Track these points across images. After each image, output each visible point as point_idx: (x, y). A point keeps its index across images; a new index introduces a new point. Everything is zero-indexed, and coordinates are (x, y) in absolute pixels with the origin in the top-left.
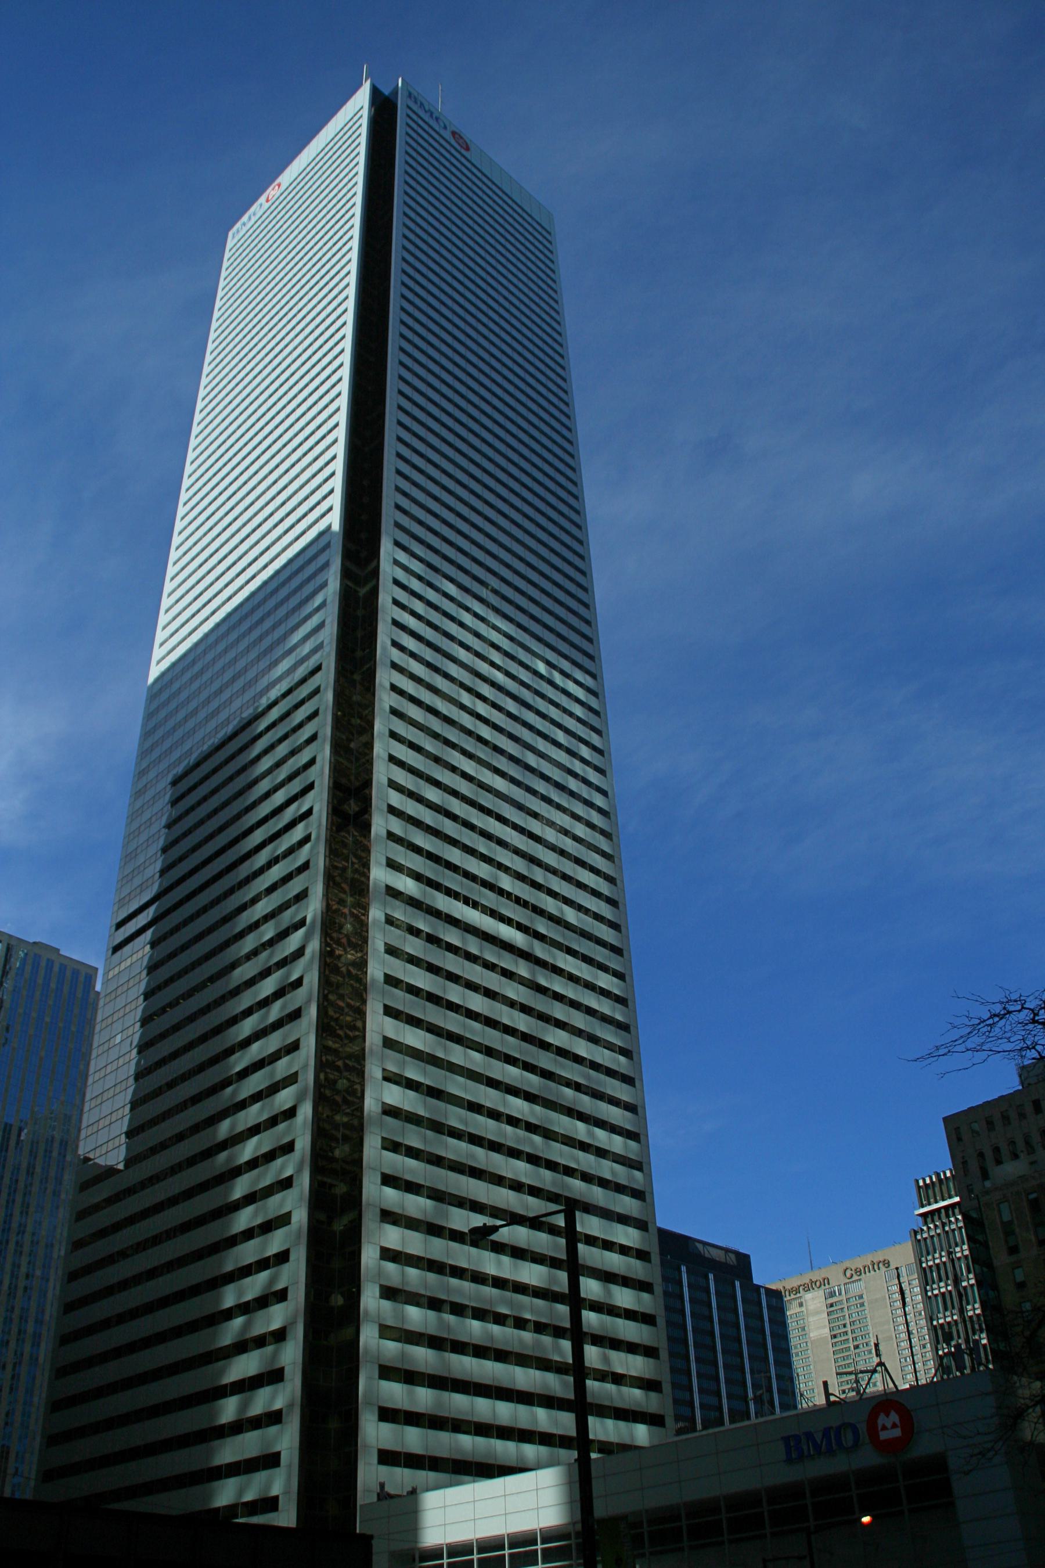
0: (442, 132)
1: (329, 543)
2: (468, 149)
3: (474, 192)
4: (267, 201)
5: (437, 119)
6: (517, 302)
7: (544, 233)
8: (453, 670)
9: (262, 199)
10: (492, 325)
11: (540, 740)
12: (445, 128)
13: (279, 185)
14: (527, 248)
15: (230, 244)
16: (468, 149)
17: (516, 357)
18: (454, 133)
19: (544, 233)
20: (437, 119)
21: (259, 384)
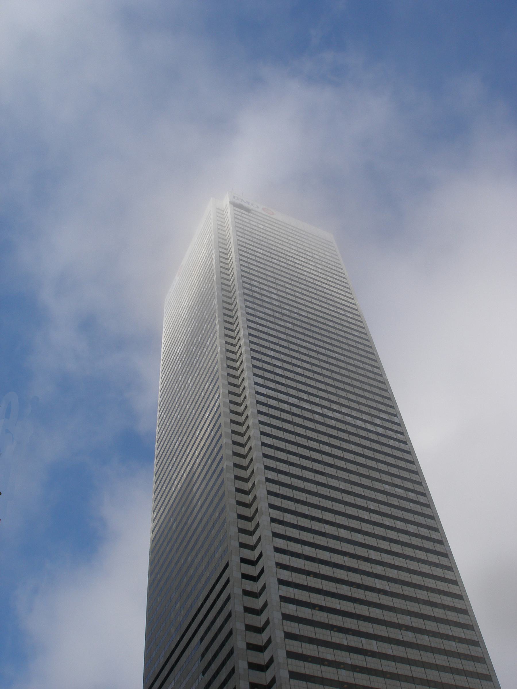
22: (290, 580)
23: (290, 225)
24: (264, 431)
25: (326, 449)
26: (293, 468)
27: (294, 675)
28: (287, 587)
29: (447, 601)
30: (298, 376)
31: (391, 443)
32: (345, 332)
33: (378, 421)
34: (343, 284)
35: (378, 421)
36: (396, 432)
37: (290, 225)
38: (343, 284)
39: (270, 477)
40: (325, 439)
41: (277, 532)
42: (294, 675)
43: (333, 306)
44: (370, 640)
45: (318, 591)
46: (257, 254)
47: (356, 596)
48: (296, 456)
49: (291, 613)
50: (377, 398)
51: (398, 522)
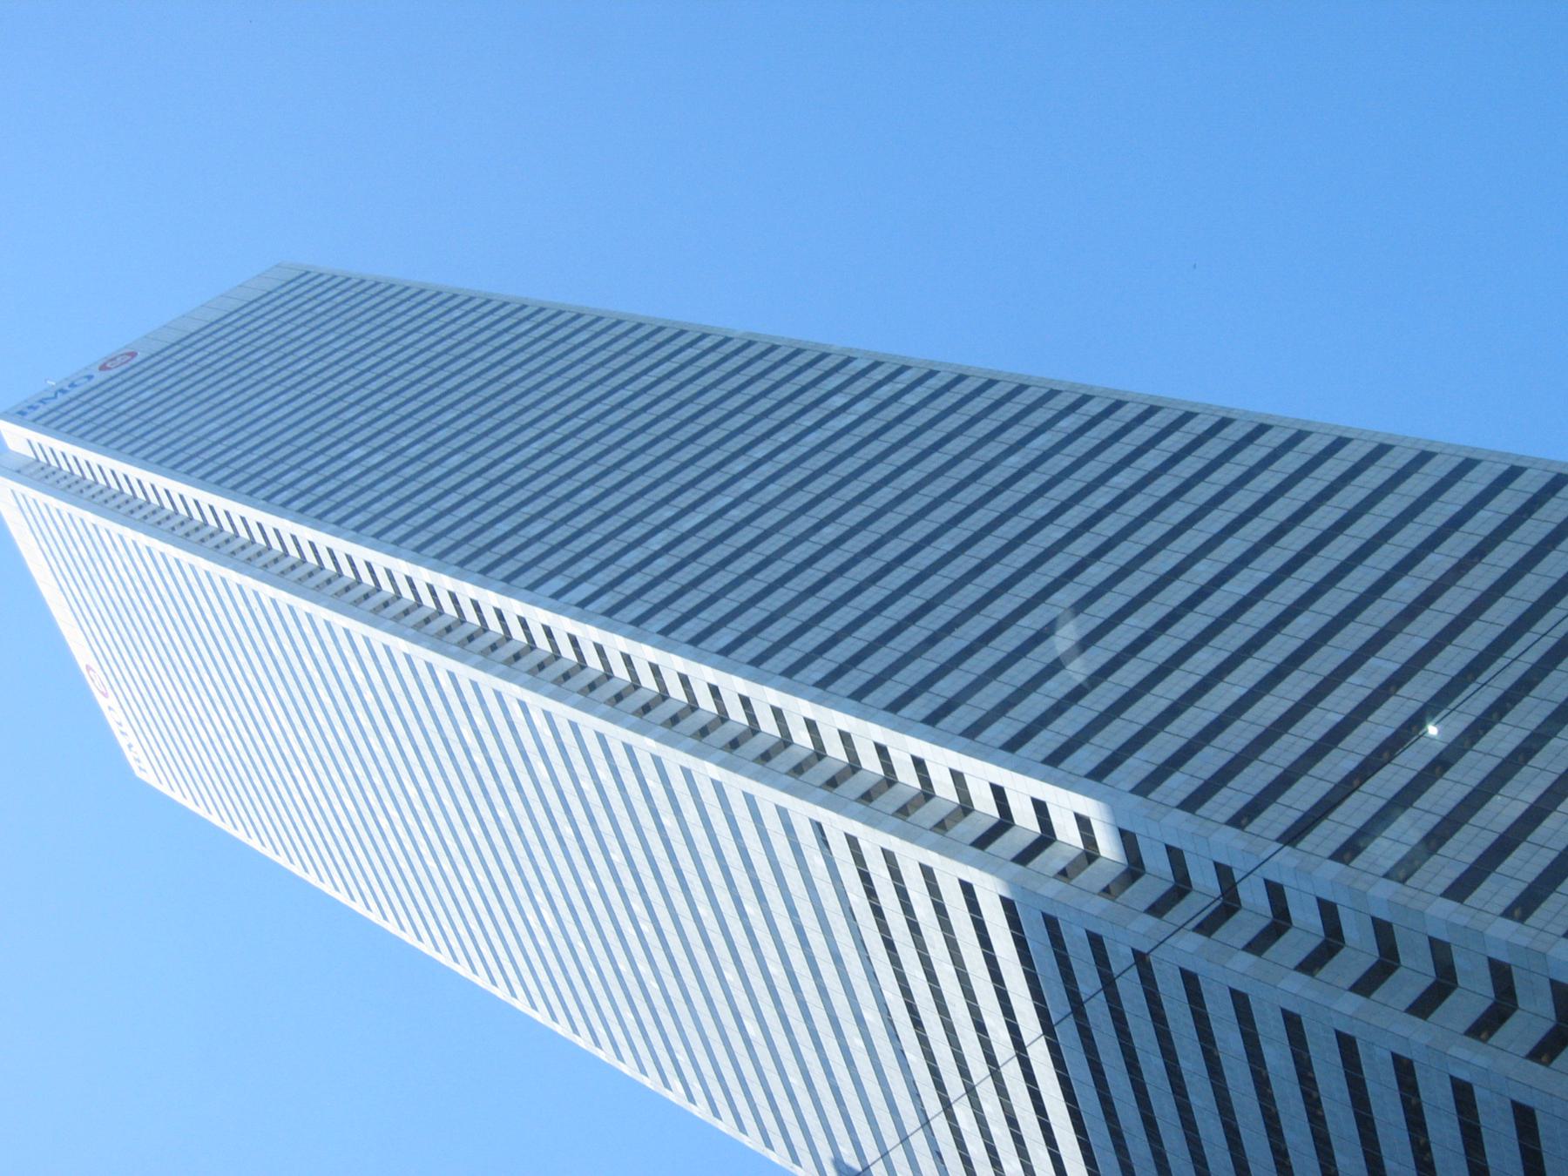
0: (93, 383)
1: (653, 756)
2: (133, 355)
3: (463, 414)
4: (106, 695)
5: (72, 385)
6: (513, 409)
7: (303, 280)
8: (331, 337)
9: (103, 703)
10: (484, 410)
11: (1199, 465)
12: (90, 377)
13: (88, 668)
14: (474, 392)
15: (149, 777)
16: (133, 355)
17: (507, 397)
18: (103, 368)
19: (303, 280)
20: (72, 385)
21: (353, 827)
22: (1107, 753)
23: (231, 314)
24: (693, 634)
25: (830, 533)
26: (920, 638)
27: (1523, 907)
28: (1121, 768)
29: (1374, 477)
30: (604, 502)
31: (910, 400)
32: (331, 378)
33: (838, 401)
34: (433, 302)
35: (838, 401)
36: (890, 378)
37: (231, 314)
38: (433, 302)
39: (818, 676)
40: (803, 524)
41: (1049, 752)
42: (1523, 907)
43: (474, 349)
44: (1364, 667)
45: (1174, 711)
46: (214, 438)
47: (1191, 634)
48: (1124, 662)
49: (1191, 789)
50: (778, 375)
51: (1115, 480)
